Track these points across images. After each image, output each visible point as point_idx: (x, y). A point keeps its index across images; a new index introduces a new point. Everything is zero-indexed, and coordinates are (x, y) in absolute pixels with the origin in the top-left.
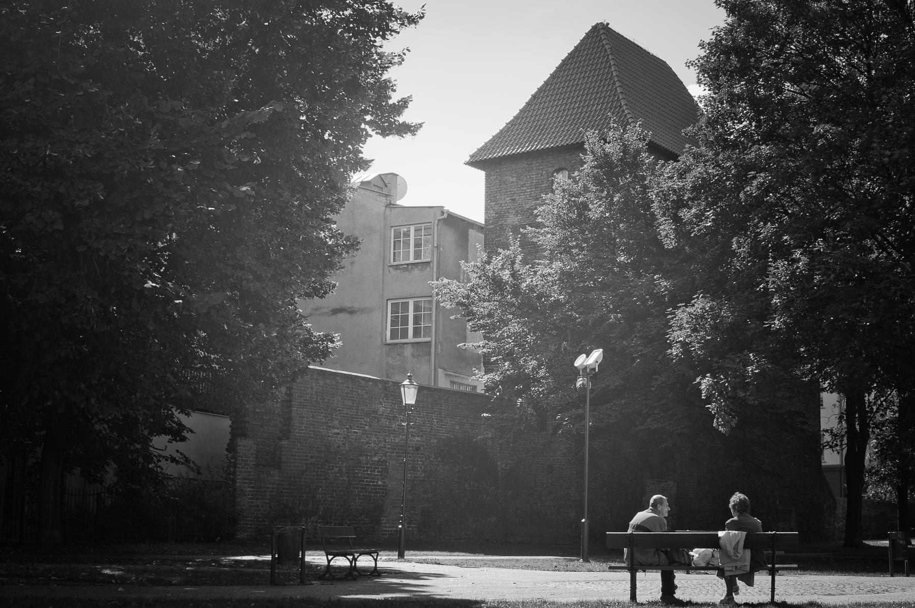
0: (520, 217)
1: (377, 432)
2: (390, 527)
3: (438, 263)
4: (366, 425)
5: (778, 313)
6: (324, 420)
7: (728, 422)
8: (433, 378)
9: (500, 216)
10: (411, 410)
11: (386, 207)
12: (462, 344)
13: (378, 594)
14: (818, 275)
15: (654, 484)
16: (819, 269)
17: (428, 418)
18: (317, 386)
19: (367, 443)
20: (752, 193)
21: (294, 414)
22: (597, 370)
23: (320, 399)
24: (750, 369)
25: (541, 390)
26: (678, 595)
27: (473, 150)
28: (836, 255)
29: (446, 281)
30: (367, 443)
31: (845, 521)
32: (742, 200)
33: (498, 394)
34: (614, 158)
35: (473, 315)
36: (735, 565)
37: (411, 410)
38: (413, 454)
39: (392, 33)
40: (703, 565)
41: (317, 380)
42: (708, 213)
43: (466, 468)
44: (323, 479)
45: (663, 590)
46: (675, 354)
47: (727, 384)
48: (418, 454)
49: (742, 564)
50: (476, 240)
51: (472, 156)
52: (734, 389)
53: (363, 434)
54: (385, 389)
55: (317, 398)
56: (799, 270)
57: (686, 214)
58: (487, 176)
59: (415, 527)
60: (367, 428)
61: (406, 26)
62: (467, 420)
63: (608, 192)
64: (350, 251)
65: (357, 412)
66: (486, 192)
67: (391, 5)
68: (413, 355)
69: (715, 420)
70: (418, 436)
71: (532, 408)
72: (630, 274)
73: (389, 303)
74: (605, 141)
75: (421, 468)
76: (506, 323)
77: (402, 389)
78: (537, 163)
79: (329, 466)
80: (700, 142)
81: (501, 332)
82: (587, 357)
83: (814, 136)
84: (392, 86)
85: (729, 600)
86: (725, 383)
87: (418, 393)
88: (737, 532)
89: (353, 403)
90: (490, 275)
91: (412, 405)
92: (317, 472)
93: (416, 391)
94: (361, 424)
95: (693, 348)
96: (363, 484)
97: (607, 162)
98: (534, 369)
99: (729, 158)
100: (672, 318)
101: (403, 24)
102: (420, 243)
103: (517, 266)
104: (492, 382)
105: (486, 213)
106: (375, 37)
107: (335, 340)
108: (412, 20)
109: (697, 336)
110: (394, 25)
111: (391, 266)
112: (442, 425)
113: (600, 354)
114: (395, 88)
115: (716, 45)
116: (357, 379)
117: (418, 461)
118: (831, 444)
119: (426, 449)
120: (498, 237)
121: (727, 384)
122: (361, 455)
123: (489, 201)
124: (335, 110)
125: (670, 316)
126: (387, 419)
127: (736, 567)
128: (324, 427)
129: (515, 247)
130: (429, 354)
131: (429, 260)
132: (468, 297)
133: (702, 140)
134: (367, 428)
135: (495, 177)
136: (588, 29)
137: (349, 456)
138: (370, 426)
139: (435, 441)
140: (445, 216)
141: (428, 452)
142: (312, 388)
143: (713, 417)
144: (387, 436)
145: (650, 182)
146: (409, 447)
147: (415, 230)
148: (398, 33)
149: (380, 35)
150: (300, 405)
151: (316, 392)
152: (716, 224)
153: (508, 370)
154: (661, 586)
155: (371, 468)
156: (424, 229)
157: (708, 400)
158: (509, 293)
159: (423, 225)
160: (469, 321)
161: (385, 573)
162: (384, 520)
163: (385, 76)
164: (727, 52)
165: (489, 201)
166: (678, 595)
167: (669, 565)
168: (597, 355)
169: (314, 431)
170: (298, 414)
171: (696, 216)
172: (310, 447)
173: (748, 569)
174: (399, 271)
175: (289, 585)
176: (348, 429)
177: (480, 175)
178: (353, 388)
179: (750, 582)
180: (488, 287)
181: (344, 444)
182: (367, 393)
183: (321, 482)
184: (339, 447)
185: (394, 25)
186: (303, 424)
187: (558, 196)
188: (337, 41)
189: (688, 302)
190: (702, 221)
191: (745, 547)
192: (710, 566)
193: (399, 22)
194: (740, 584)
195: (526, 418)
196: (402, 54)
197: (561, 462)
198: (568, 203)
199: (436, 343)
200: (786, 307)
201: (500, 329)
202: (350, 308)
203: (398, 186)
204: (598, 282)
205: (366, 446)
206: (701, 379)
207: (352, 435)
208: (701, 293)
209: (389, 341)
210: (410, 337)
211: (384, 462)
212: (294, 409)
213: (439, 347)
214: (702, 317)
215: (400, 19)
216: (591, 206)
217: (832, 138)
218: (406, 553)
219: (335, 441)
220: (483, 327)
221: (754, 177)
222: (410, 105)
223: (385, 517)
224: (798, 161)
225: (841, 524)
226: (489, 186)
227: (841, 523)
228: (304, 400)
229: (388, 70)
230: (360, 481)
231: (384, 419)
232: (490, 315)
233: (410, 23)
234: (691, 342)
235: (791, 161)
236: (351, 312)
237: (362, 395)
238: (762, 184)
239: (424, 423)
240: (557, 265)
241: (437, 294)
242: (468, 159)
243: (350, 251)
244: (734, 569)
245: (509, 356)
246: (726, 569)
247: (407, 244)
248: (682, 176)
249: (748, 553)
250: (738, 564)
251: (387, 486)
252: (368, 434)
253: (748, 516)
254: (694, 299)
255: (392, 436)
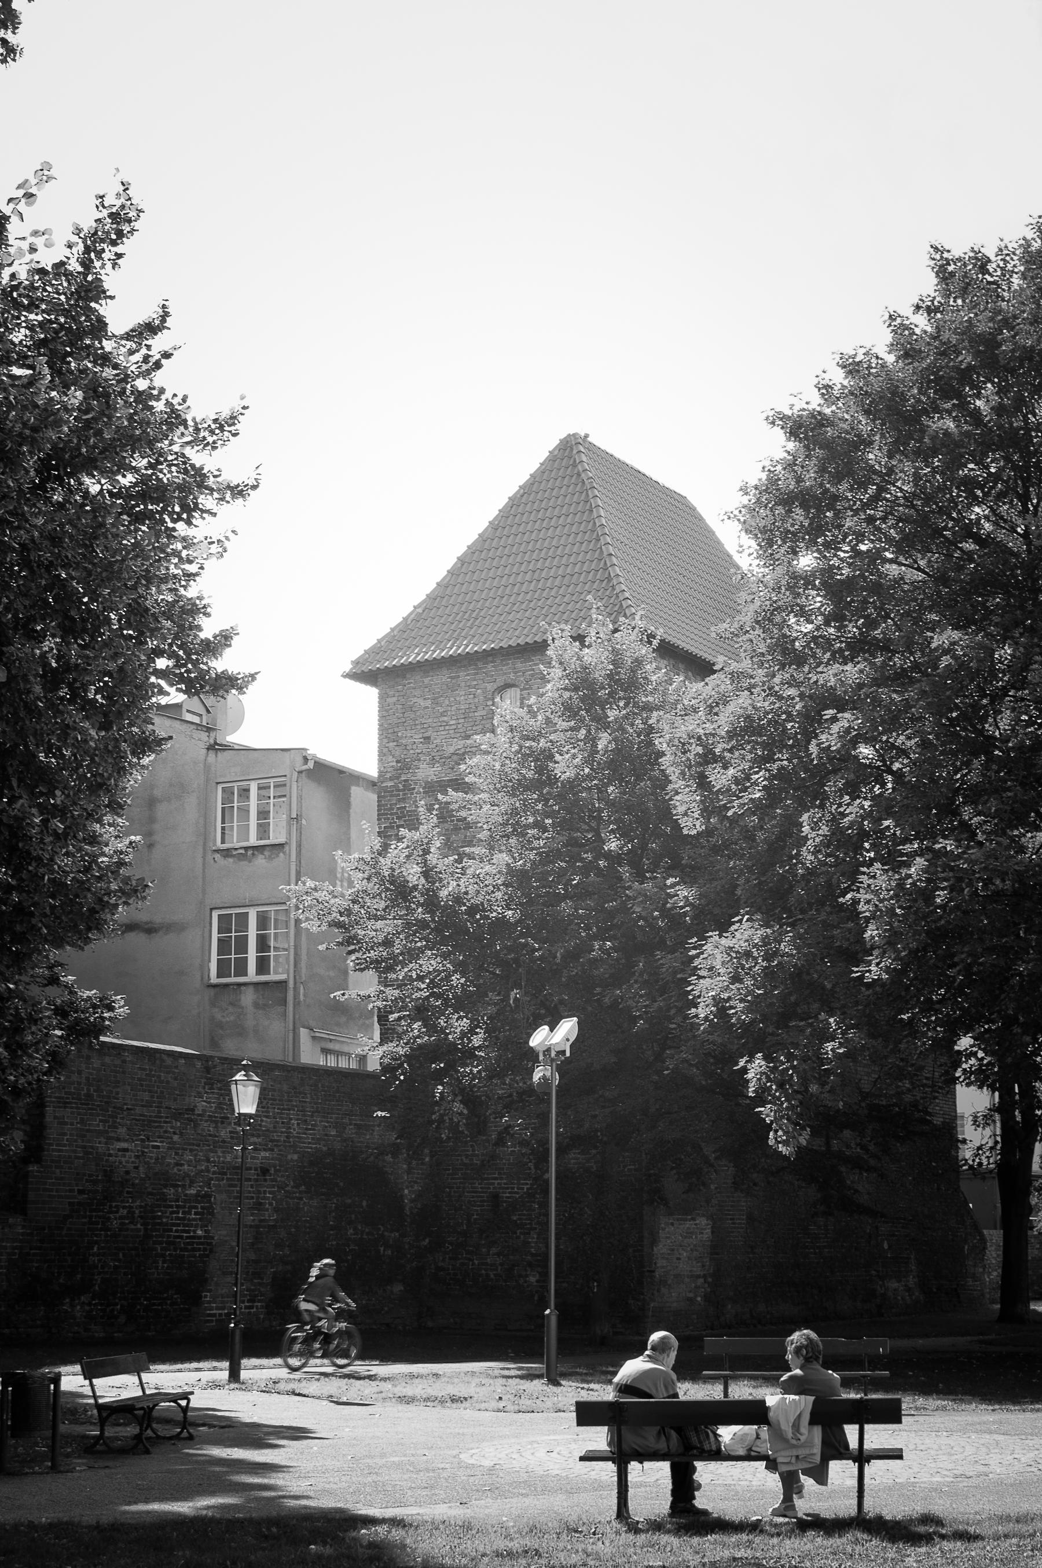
0: (437, 767)
1: (193, 1144)
2: (217, 1308)
3: (299, 846)
4: (175, 1133)
5: (876, 952)
6: (101, 1128)
7: (794, 1137)
8: (291, 1046)
9: (404, 765)
10: (249, 1124)
11: (208, 749)
12: (339, 993)
13: (185, 1499)
14: (943, 889)
15: (672, 1224)
16: (945, 879)
17: (281, 1118)
18: (88, 1068)
19: (177, 1164)
20: (830, 746)
21: (48, 1119)
22: (568, 1054)
23: (95, 1091)
24: (829, 1046)
25: (475, 1070)
26: (700, 1502)
27: (357, 653)
28: (973, 857)
29: (310, 883)
30: (177, 1164)
31: (1000, 1271)
32: (813, 756)
33: (402, 1078)
34: (599, 675)
35: (358, 942)
36: (795, 1453)
37: (249, 1124)
38: (256, 1180)
39: (205, 515)
40: (742, 1452)
41: (88, 1058)
42: (757, 776)
43: (349, 1201)
44: (101, 1229)
45: (674, 1492)
46: (702, 1016)
47: (791, 1072)
48: (265, 1180)
49: (808, 1452)
50: (363, 801)
51: (356, 663)
52: (805, 1081)
53: (169, 1148)
54: (208, 1070)
55: (89, 1090)
56: (910, 881)
57: (720, 778)
58: (382, 698)
59: (262, 1307)
60: (176, 1138)
61: (228, 502)
62: (350, 1120)
63: (589, 731)
64: (131, 901)
65: (159, 1112)
66: (381, 725)
67: (202, 468)
68: (256, 1005)
69: (771, 1133)
70: (265, 1150)
71: (461, 1102)
72: (625, 872)
73: (215, 915)
74: (583, 645)
75: (271, 1204)
76: (413, 955)
77: (233, 1087)
78: (468, 675)
79: (111, 1206)
80: (743, 655)
81: (406, 970)
82: (552, 1030)
83: (936, 649)
84: (205, 607)
85: (786, 1508)
86: (787, 1069)
87: (260, 1094)
88: (797, 1397)
89: (152, 1097)
90: (386, 874)
91: (250, 1116)
92: (91, 1217)
93: (258, 1091)
94: (166, 1132)
95: (733, 1011)
96: (169, 1236)
97: (585, 680)
98: (463, 1034)
99: (792, 683)
100: (697, 956)
101: (222, 499)
102: (266, 809)
103: (433, 858)
104: (392, 1059)
105: (380, 760)
106: (174, 521)
107: (117, 1006)
108: (238, 492)
109: (738, 989)
110: (206, 501)
111: (217, 851)
112: (307, 1129)
113: (572, 1027)
114: (209, 610)
115: (768, 488)
116: (158, 1055)
117: (265, 1192)
118: (970, 1162)
119: (279, 1171)
120: (399, 801)
121: (791, 1072)
122: (165, 1186)
123: (386, 741)
124: (104, 658)
125: (693, 952)
126: (212, 1121)
127: (797, 1457)
128: (103, 1140)
129: (428, 826)
130: (284, 1002)
131: (282, 840)
132: (348, 912)
133: (745, 651)
134: (176, 1138)
135: (395, 699)
136: (553, 443)
137: (146, 1188)
138: (181, 1134)
139: (295, 1157)
140: (311, 765)
141: (282, 1176)
142: (80, 1072)
143: (769, 1127)
144: (211, 1151)
145: (658, 721)
146: (250, 1169)
147: (259, 788)
148: (214, 515)
149: (182, 519)
150: (59, 1102)
151: (87, 1079)
152: (769, 794)
153: (418, 1037)
154: (670, 1487)
155: (184, 1207)
156: (275, 787)
157: (761, 1099)
158: (419, 904)
159: (272, 781)
160: (350, 953)
161: (203, 1425)
162: (207, 1296)
163: (191, 592)
164: (787, 501)
165: (386, 741)
166: (700, 1502)
167: (683, 1455)
168: (567, 1028)
169: (84, 1147)
170: (55, 1117)
171: (737, 781)
172: (78, 1174)
173: (818, 1459)
174: (231, 860)
175: (34, 1473)
176: (142, 1141)
177: (370, 695)
178: (151, 1070)
179: (820, 1475)
180: (383, 895)
181: (136, 1168)
182: (176, 1079)
183: (96, 1236)
184: (127, 1173)
185: (206, 501)
186: (65, 1134)
187: (502, 738)
188: (107, 538)
189: (723, 927)
190: (745, 790)
191: (812, 1422)
192: (753, 1454)
193: (216, 495)
194: (808, 1482)
195: (451, 1119)
196: (223, 539)
197: (513, 1188)
198: (518, 752)
199: (295, 983)
200: (891, 940)
201: (404, 964)
202: (147, 923)
203: (229, 711)
204: (571, 885)
205: (175, 1170)
206: (747, 1062)
207: (150, 1152)
208: (747, 913)
209: (214, 979)
210: (251, 973)
211: (208, 1196)
212: (49, 1109)
213: (302, 991)
214: (748, 954)
215: (219, 490)
216: (558, 757)
217: (964, 655)
218: (245, 1362)
219: (120, 1163)
220: (376, 963)
221: (834, 719)
222: (235, 641)
223: (210, 1291)
224: (907, 691)
225: (994, 1275)
226: (384, 713)
227: (995, 1273)
228: (66, 1093)
229: (197, 578)
230: (165, 1230)
231: (206, 1121)
232: (387, 943)
233: (233, 497)
234: (729, 998)
235: (895, 691)
236: (150, 930)
237: (168, 1082)
238: (848, 731)
239: (275, 1127)
240: (502, 858)
241: (297, 908)
242: (348, 667)
243: (131, 901)
244: (793, 1460)
245: (421, 1012)
246: (779, 1460)
247: (245, 812)
248: (712, 710)
249: (817, 1432)
250: (802, 1452)
251: (213, 1238)
252: (179, 1149)
253: (817, 1370)
254: (733, 923)
255: (219, 1151)
